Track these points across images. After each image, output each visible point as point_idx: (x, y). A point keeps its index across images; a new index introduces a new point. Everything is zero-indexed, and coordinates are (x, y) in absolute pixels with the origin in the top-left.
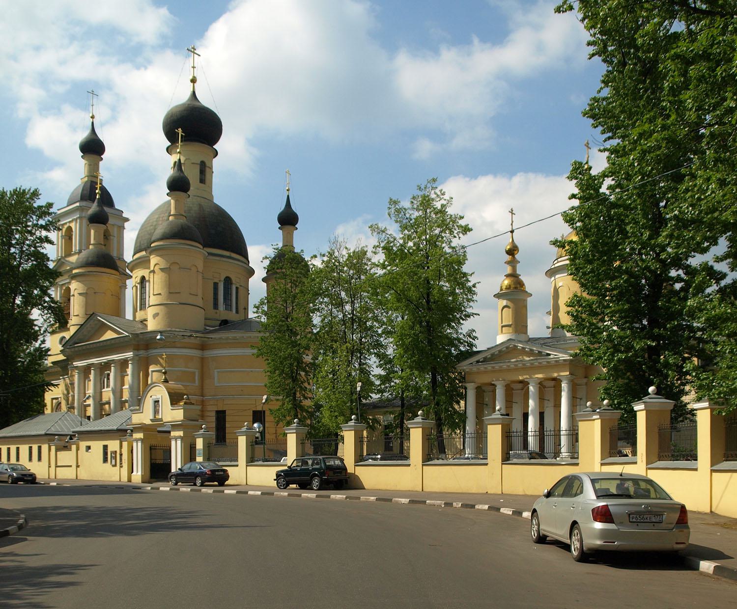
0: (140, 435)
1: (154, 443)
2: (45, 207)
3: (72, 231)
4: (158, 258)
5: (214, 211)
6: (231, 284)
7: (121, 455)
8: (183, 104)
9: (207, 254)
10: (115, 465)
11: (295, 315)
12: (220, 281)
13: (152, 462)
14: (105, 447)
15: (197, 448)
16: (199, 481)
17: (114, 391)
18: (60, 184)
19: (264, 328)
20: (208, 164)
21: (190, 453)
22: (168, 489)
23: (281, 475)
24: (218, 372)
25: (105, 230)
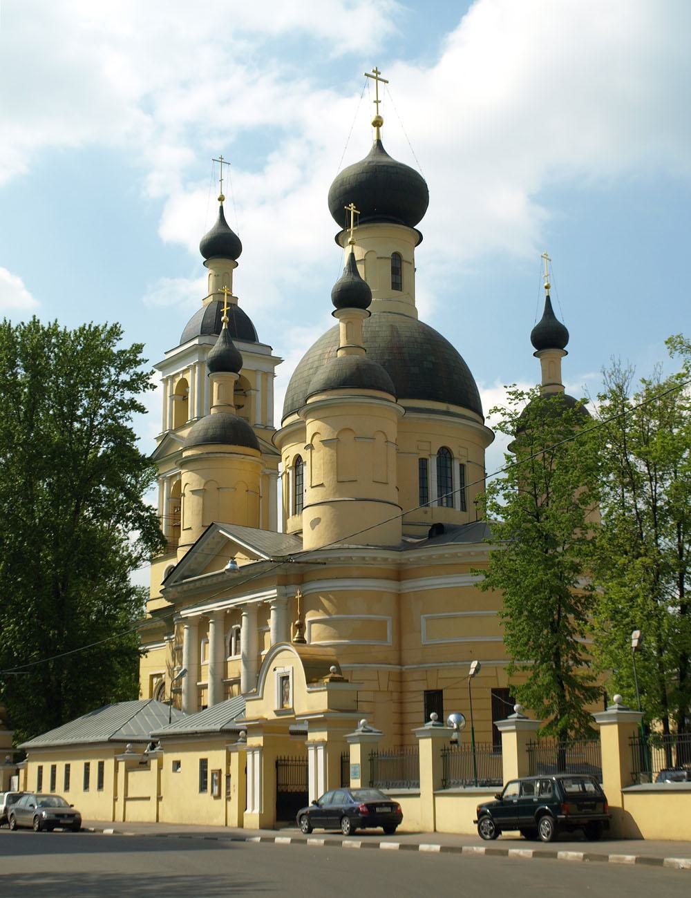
0: (256, 741)
1: (283, 753)
2: (129, 352)
3: (188, 387)
4: (318, 423)
5: (416, 335)
6: (451, 459)
7: (228, 777)
8: (360, 164)
9: (403, 411)
10: (218, 797)
11: (552, 509)
12: (430, 455)
13: (280, 789)
14: (204, 763)
15: (351, 762)
16: (346, 826)
17: (246, 661)
18: (158, 316)
19: (497, 535)
20: (405, 257)
21: (340, 772)
22: (288, 840)
23: (485, 813)
24: (427, 619)
25: (236, 382)
